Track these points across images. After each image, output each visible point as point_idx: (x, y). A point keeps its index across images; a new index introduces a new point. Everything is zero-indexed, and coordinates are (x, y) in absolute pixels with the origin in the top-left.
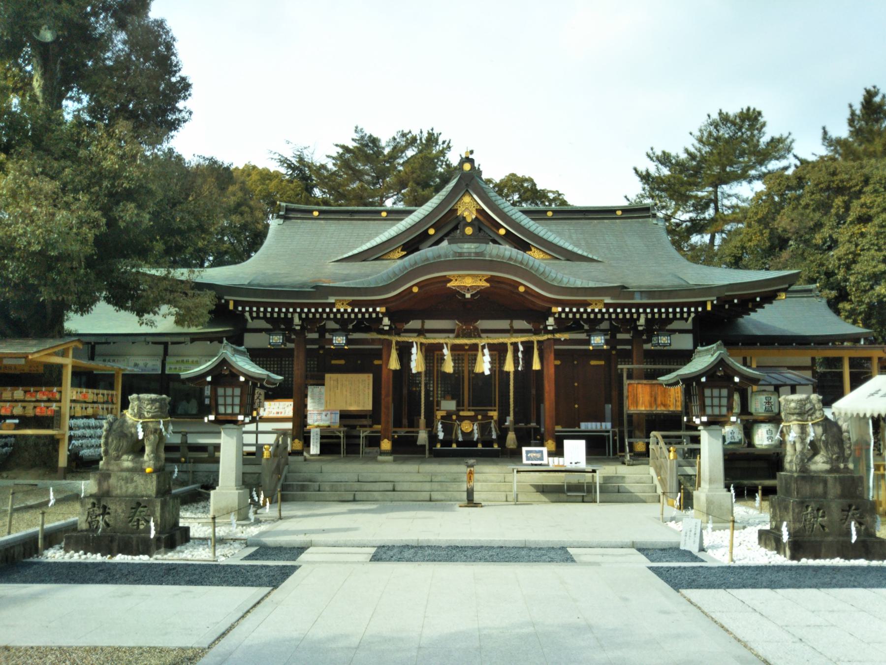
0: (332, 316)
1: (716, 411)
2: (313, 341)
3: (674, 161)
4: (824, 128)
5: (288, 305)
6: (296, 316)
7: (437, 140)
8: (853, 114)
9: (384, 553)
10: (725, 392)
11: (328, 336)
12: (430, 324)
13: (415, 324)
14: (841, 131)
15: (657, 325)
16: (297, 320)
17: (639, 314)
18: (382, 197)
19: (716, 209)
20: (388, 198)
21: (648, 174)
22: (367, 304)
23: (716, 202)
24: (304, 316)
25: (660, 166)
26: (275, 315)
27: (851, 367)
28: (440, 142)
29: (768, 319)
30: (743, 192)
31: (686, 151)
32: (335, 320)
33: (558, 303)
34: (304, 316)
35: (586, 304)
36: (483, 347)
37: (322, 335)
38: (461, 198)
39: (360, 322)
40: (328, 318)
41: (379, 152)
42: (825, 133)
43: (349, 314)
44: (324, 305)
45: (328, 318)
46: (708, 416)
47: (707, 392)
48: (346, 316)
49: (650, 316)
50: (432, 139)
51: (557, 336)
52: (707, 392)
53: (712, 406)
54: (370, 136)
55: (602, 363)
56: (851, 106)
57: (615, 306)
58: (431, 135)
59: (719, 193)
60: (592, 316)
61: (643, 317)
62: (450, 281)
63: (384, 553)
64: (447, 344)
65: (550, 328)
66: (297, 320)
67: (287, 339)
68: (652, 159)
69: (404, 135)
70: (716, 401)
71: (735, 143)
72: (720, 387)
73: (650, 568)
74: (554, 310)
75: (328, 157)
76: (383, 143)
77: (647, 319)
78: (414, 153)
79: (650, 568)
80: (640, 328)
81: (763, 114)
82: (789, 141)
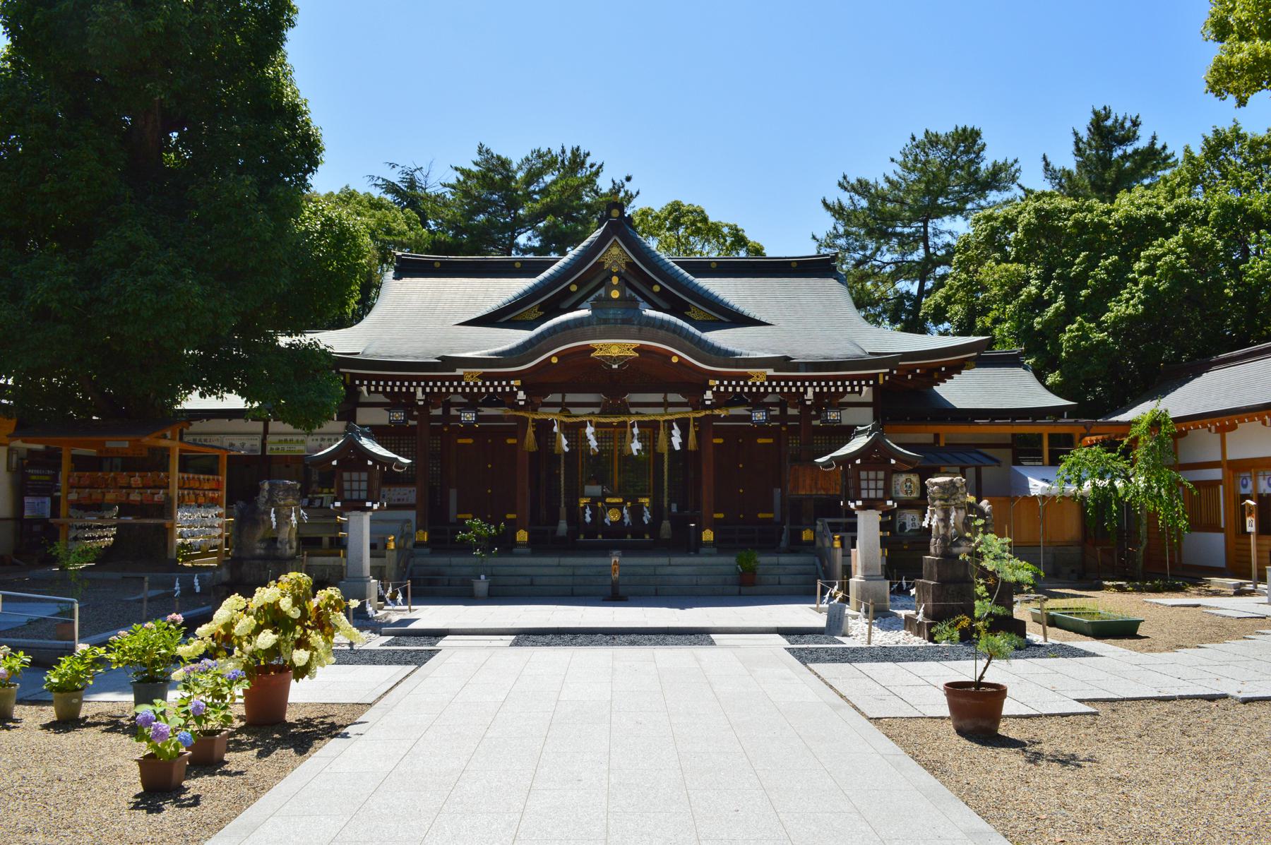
0: (460, 390)
1: (872, 494)
2: (437, 418)
3: (873, 191)
4: (1045, 158)
5: (410, 379)
6: (420, 389)
7: (583, 163)
8: (1078, 140)
9: (526, 636)
10: (881, 475)
11: (453, 412)
12: (570, 398)
13: (555, 397)
14: (1067, 161)
15: (826, 401)
16: (420, 395)
17: (806, 388)
18: (513, 233)
19: (927, 248)
20: (520, 233)
21: (841, 207)
22: (500, 377)
23: (925, 239)
24: (428, 390)
25: (856, 197)
26: (396, 389)
27: (1050, 444)
28: (587, 165)
29: (961, 391)
30: (954, 229)
31: (888, 180)
32: (464, 394)
33: (715, 375)
34: (428, 390)
35: (746, 377)
36: (632, 426)
37: (446, 411)
38: (608, 250)
39: (491, 395)
40: (456, 392)
41: (509, 178)
42: (1047, 164)
43: (480, 388)
44: (451, 379)
45: (456, 392)
46: (863, 500)
47: (863, 474)
48: (476, 390)
49: (817, 389)
50: (577, 160)
51: (717, 412)
52: (863, 474)
53: (868, 489)
54: (499, 158)
55: (770, 441)
56: (1076, 134)
57: (778, 379)
58: (576, 152)
59: (930, 230)
60: (754, 389)
61: (810, 390)
62: (594, 350)
63: (526, 636)
64: (591, 422)
65: (708, 403)
66: (420, 395)
67: (409, 416)
68: (846, 189)
69: (540, 156)
70: (872, 485)
71: (952, 169)
72: (876, 470)
73: (788, 649)
74: (711, 382)
75: (445, 186)
76: (514, 166)
77: (815, 393)
78: (554, 178)
79: (788, 649)
80: (808, 403)
81: (983, 135)
82: (1013, 169)
